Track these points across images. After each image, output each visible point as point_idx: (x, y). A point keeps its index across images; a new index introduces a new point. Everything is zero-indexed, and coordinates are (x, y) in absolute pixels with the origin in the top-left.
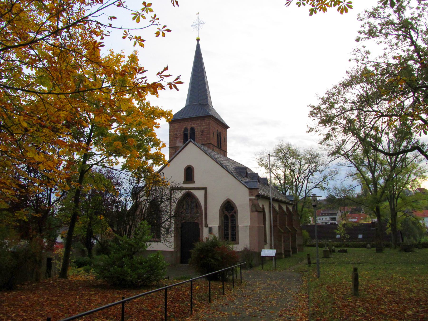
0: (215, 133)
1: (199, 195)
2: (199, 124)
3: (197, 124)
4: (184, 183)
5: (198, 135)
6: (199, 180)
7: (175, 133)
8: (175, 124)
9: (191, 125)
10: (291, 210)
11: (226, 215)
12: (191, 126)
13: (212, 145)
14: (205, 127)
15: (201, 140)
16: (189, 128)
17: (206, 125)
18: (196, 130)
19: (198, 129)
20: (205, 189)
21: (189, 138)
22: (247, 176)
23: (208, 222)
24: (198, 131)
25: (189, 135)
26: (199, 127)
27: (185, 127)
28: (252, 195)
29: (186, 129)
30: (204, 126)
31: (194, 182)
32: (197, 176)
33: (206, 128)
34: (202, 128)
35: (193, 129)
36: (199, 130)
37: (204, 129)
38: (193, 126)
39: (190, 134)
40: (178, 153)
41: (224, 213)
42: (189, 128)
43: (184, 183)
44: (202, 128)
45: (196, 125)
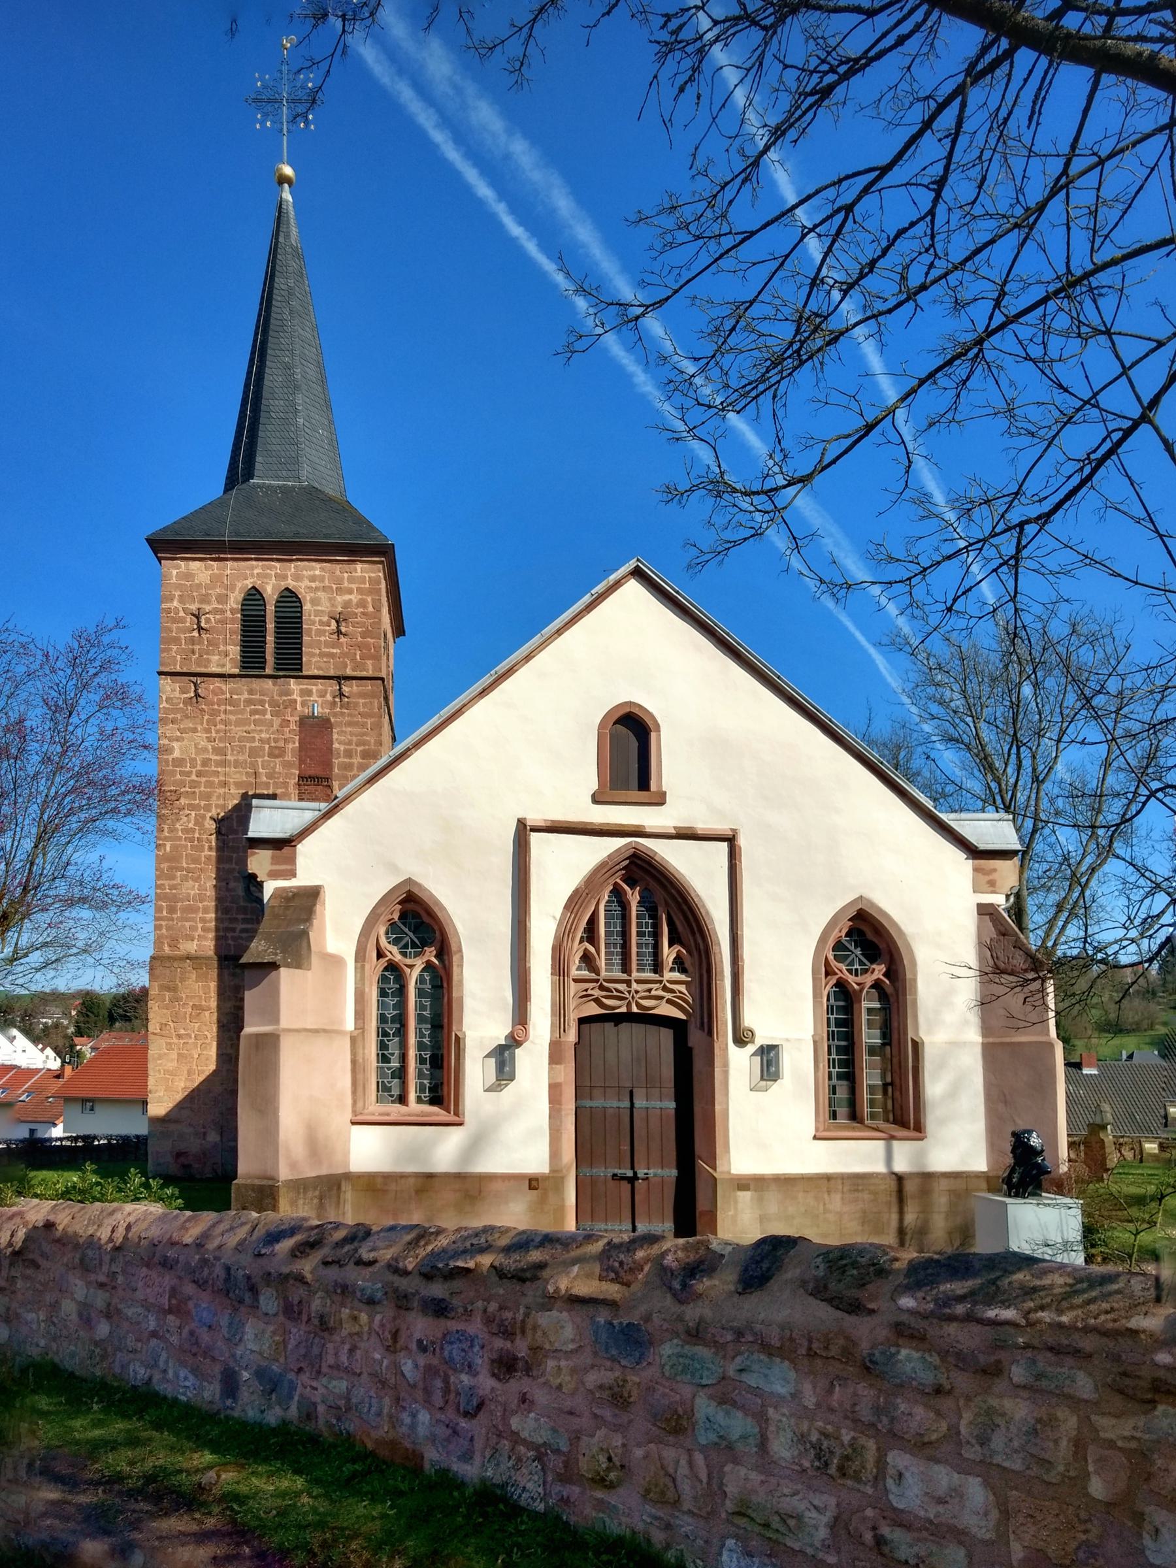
1: (699, 871)
2: (322, 579)
4: (596, 800)
5: (320, 633)
7: (193, 607)
11: (841, 985)
12: (283, 585)
14: (354, 598)
15: (332, 655)
16: (270, 592)
18: (307, 607)
23: (749, 1019)
24: (317, 613)
25: (270, 626)
26: (320, 594)
27: (249, 583)
28: (992, 886)
29: (254, 597)
30: (350, 592)
31: (660, 800)
32: (672, 761)
33: (362, 604)
35: (290, 600)
36: (325, 606)
37: (347, 604)
38: (291, 583)
39: (279, 620)
42: (270, 592)
43: (596, 800)
45: (306, 583)
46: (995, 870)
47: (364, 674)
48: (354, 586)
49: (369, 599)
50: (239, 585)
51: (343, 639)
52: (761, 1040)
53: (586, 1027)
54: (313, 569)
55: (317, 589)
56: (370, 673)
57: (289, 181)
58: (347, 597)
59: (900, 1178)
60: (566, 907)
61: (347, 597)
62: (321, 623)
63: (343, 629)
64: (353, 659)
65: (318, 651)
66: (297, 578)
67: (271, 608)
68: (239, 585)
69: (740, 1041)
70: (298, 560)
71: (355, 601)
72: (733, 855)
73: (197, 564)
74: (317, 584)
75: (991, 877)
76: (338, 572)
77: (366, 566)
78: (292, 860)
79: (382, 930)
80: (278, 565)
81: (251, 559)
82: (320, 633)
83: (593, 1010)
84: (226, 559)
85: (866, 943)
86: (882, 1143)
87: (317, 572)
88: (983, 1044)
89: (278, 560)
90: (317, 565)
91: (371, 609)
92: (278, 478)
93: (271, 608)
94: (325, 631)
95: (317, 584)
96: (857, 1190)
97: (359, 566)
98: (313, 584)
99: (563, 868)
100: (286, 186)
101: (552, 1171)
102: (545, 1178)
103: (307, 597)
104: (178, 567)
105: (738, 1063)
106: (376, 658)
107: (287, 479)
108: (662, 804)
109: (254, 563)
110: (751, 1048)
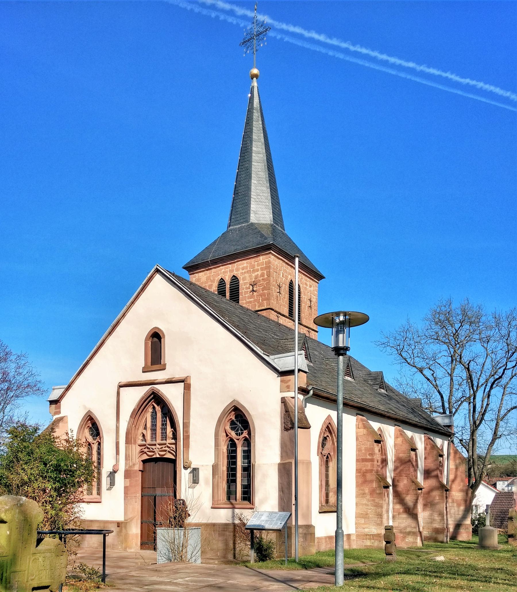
0: (285, 289)
1: (173, 395)
2: (247, 267)
3: (243, 269)
6: (175, 361)
8: (201, 274)
9: (232, 271)
10: (386, 392)
11: (231, 440)
13: (276, 311)
14: (259, 273)
15: (250, 302)
17: (262, 269)
18: (241, 282)
19: (244, 279)
20: (185, 381)
21: (341, 373)
22: (288, 474)
29: (222, 282)
30: (258, 270)
34: (253, 275)
35: (235, 280)
36: (248, 281)
37: (256, 277)
38: (235, 273)
40: (133, 303)
41: (227, 435)
42: (228, 280)
44: (253, 275)
46: (290, 380)
47: (263, 308)
48: (259, 267)
49: (265, 272)
50: (216, 279)
51: (255, 294)
52: (193, 466)
53: (147, 464)
54: (244, 264)
55: (245, 272)
56: (265, 307)
57: (256, 76)
58: (256, 273)
59: (234, 525)
60: (131, 417)
61: (256, 273)
62: (247, 288)
63: (255, 289)
64: (259, 302)
65: (245, 301)
66: (237, 270)
67: (228, 286)
68: (216, 279)
69: (185, 468)
70: (237, 261)
71: (259, 274)
72: (187, 388)
73: (202, 273)
74: (245, 270)
75: (288, 384)
76: (253, 263)
77: (264, 256)
78: (59, 407)
79: (228, 428)
80: (230, 266)
81: (220, 266)
82: (246, 293)
83: (145, 457)
84: (211, 269)
85: (239, 419)
86: (231, 510)
87: (245, 265)
88: (279, 464)
89: (230, 264)
90: (245, 262)
91: (266, 276)
92: (239, 224)
93: (228, 286)
94: (248, 292)
95: (245, 270)
96: (224, 531)
97: (261, 258)
98: (243, 271)
99: (133, 397)
100: (255, 79)
101: (125, 520)
102: (122, 523)
103: (240, 277)
104: (195, 277)
105: (184, 476)
106: (268, 299)
107: (242, 223)
108: (165, 369)
109: (222, 267)
110: (189, 470)
